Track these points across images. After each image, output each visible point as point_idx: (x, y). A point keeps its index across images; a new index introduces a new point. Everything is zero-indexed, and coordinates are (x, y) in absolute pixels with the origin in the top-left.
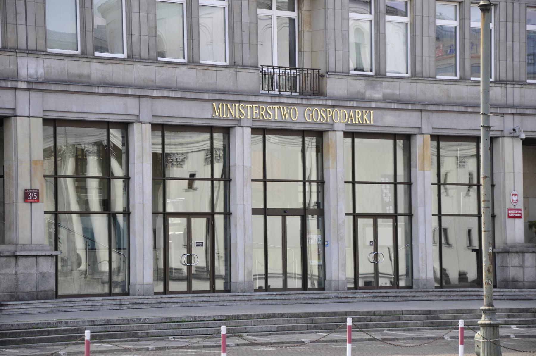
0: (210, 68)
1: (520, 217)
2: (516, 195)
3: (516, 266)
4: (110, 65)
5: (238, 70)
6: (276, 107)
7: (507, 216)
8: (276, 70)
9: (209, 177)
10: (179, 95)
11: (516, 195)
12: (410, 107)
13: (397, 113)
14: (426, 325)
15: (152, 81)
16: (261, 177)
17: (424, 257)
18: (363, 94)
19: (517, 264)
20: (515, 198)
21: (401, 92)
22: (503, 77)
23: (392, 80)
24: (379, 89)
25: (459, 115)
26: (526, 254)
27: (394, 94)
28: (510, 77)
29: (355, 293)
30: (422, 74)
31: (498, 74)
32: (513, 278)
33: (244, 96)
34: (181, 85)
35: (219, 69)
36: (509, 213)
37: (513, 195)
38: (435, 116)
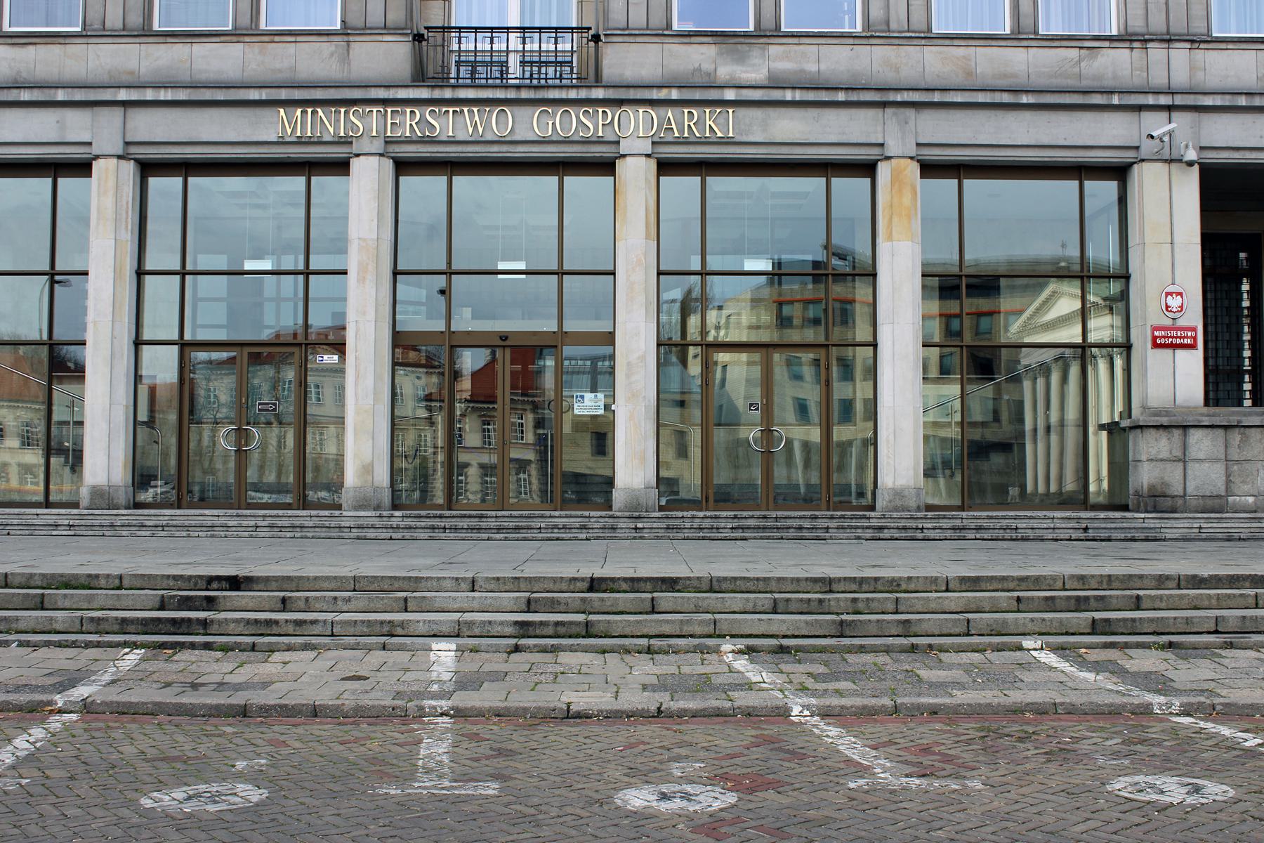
0: (277, 39)
1: (1192, 347)
2: (1181, 294)
3: (1162, 460)
4: (31, 48)
5: (351, 38)
6: (451, 110)
7: (1149, 345)
8: (514, 41)
9: (47, 268)
10: (182, 95)
11: (1181, 294)
12: (841, 97)
13: (813, 112)
14: (92, 628)
15: (132, 73)
16: (566, 267)
17: (891, 437)
18: (709, 74)
19: (1164, 454)
20: (1174, 302)
21: (823, 67)
22: (1137, 25)
23: (795, 40)
24: (756, 61)
25: (1000, 114)
26: (1192, 431)
27: (802, 71)
28: (1158, 24)
29: (816, 517)
30: (888, 25)
31: (1122, 21)
32: (1152, 487)
33: (252, 91)
34: (203, 77)
35: (299, 39)
36: (1155, 338)
37: (1168, 294)
38: (928, 116)
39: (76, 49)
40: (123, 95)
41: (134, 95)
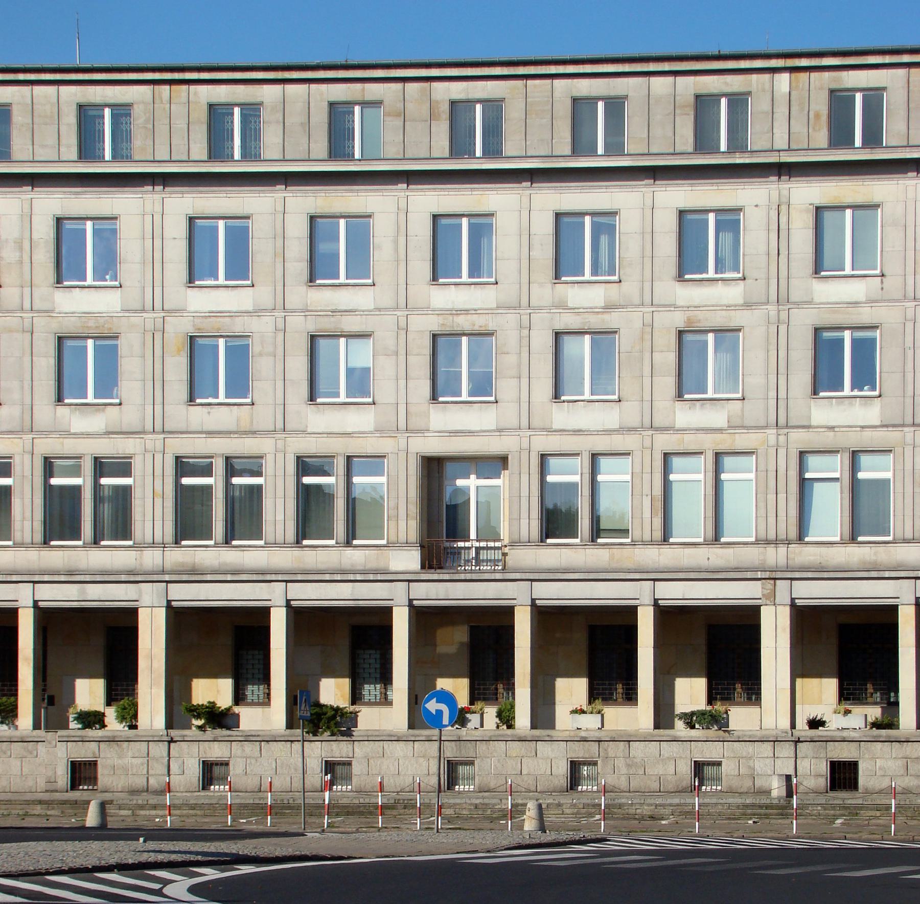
10: (255, 577)
39: (627, 551)
40: (531, 576)
41: (536, 576)
